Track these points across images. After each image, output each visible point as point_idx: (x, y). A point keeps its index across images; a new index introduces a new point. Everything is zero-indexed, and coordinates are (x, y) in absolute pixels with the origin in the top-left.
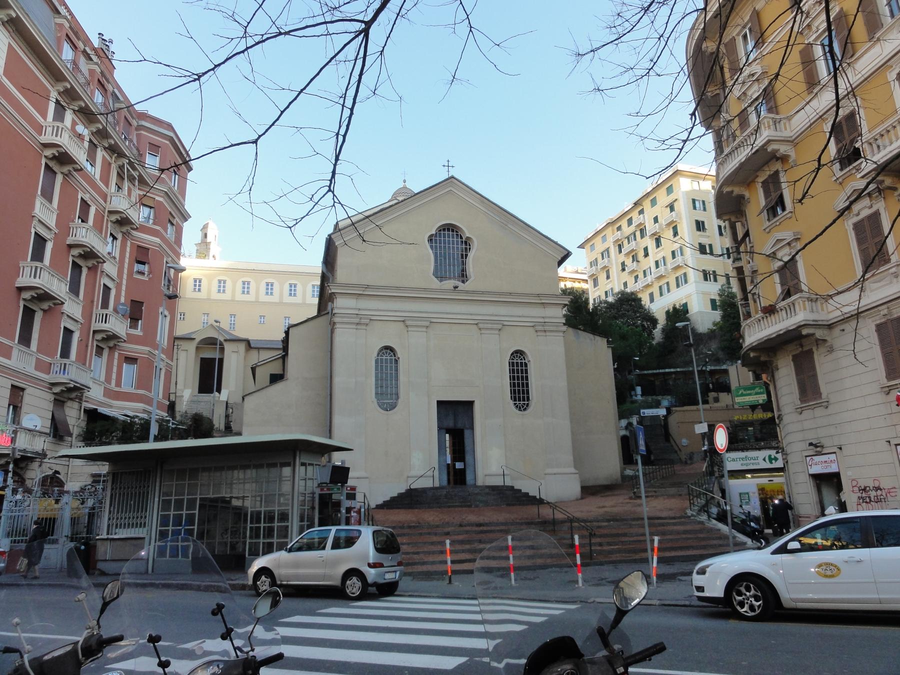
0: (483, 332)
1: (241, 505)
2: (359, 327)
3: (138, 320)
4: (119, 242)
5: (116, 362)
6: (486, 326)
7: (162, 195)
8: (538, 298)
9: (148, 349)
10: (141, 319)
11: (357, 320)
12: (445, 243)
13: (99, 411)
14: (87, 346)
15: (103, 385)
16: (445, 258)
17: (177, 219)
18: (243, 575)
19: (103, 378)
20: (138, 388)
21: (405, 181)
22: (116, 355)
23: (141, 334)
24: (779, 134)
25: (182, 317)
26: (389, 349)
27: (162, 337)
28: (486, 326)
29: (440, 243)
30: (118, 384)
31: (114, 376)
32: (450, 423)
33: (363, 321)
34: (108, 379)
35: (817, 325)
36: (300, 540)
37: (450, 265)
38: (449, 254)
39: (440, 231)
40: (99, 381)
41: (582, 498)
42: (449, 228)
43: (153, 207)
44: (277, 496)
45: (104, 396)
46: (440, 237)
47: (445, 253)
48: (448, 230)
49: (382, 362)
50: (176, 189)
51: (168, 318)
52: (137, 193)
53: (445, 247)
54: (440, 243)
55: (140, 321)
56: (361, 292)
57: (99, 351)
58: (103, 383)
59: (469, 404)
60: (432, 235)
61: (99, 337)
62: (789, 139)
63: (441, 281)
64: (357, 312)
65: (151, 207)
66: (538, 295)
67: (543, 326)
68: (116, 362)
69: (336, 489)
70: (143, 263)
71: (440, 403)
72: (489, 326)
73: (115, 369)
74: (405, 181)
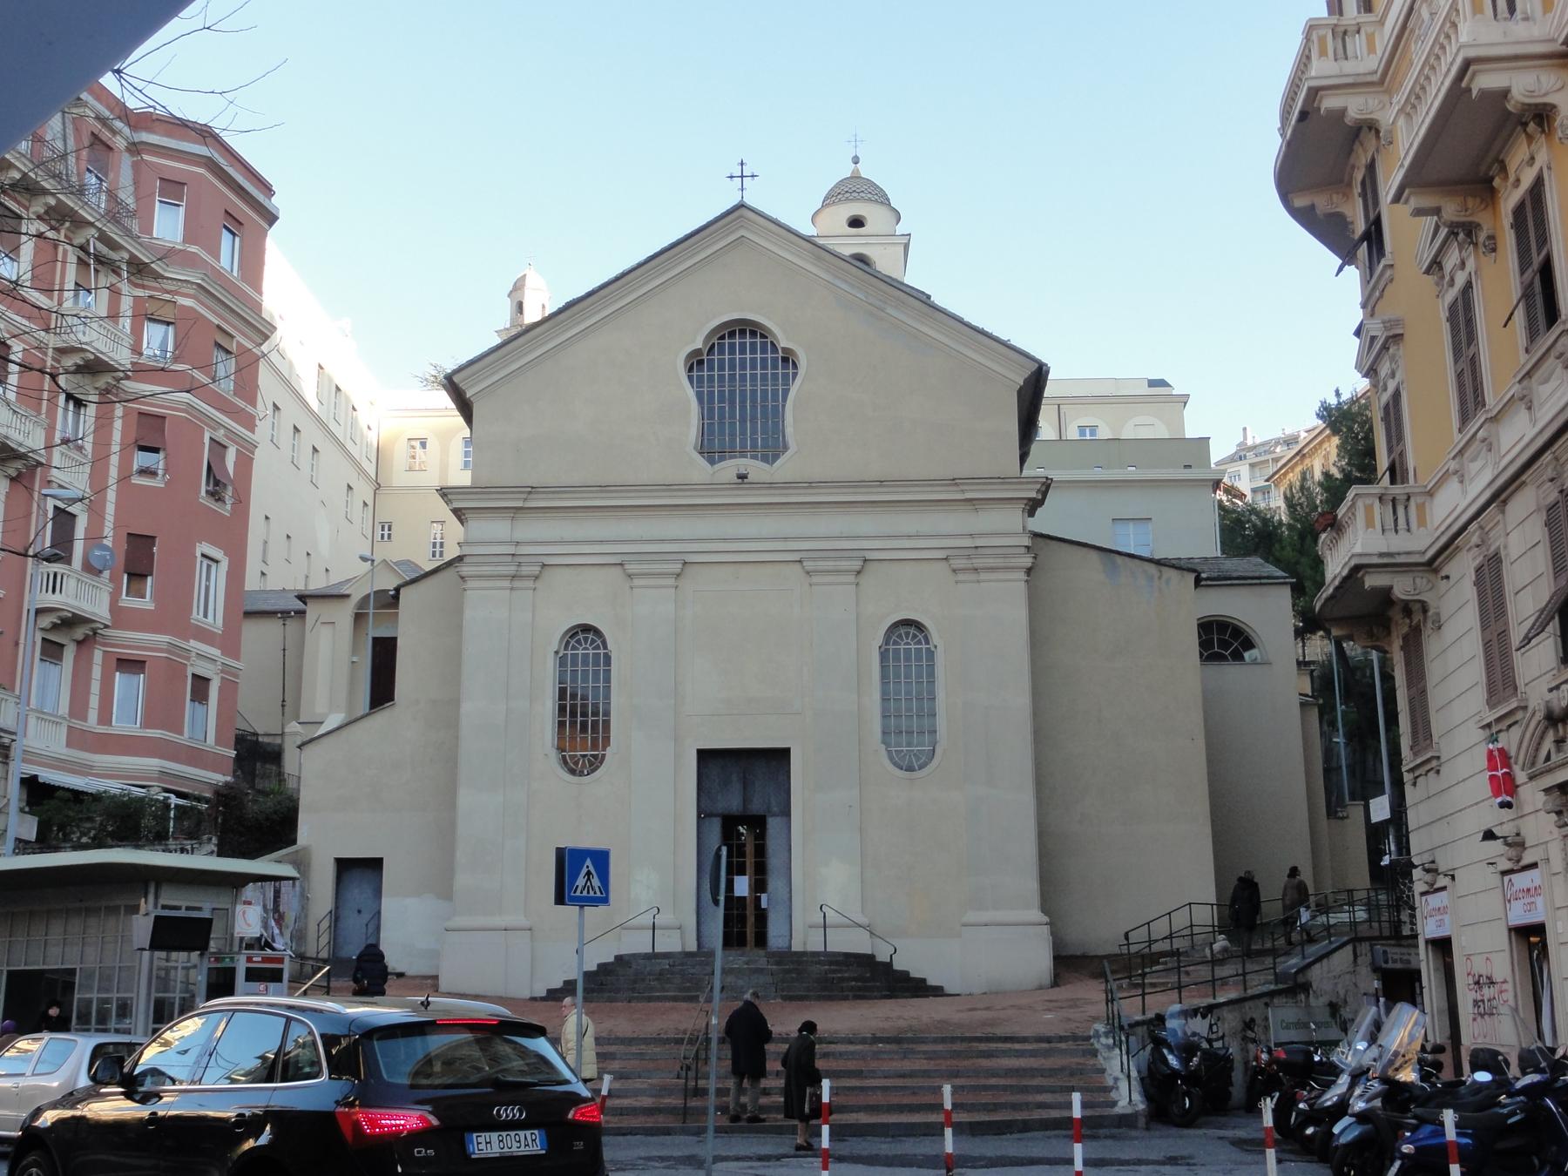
0: (815, 579)
1: (1169, 948)
2: (517, 584)
3: (146, 576)
4: (91, 410)
5: (97, 672)
6: (822, 565)
7: (192, 292)
8: (955, 488)
9: (166, 638)
10: (151, 575)
11: (512, 569)
12: (732, 367)
13: (41, 780)
14: (17, 644)
15: (65, 724)
16: (732, 403)
17: (239, 338)
18: (1257, 1157)
19: (64, 709)
20: (147, 724)
21: (856, 160)
22: (98, 656)
23: (151, 607)
24: (1349, 67)
25: (386, 532)
26: (585, 631)
27: (211, 610)
28: (822, 565)
29: (721, 368)
30: (105, 717)
31: (94, 701)
32: (732, 802)
33: (525, 570)
34: (78, 707)
35: (1391, 565)
36: (571, 1059)
37: (743, 420)
38: (743, 393)
39: (722, 338)
40: (56, 716)
41: (1052, 987)
42: (741, 331)
43: (172, 323)
44: (117, 969)
45: (69, 745)
46: (721, 352)
47: (732, 393)
48: (743, 332)
49: (574, 663)
50: (235, 275)
51: (224, 565)
52: (129, 294)
53: (732, 377)
54: (721, 368)
55: (149, 579)
56: (519, 504)
57: (52, 651)
58: (64, 718)
59: (780, 757)
60: (697, 352)
61: (46, 621)
62: (1369, 79)
63: (712, 462)
64: (511, 550)
65: (168, 324)
66: (954, 482)
67: (969, 557)
68: (97, 672)
69: (227, 960)
70: (155, 450)
71: (704, 756)
72: (830, 565)
73: (95, 687)
74: (856, 160)
